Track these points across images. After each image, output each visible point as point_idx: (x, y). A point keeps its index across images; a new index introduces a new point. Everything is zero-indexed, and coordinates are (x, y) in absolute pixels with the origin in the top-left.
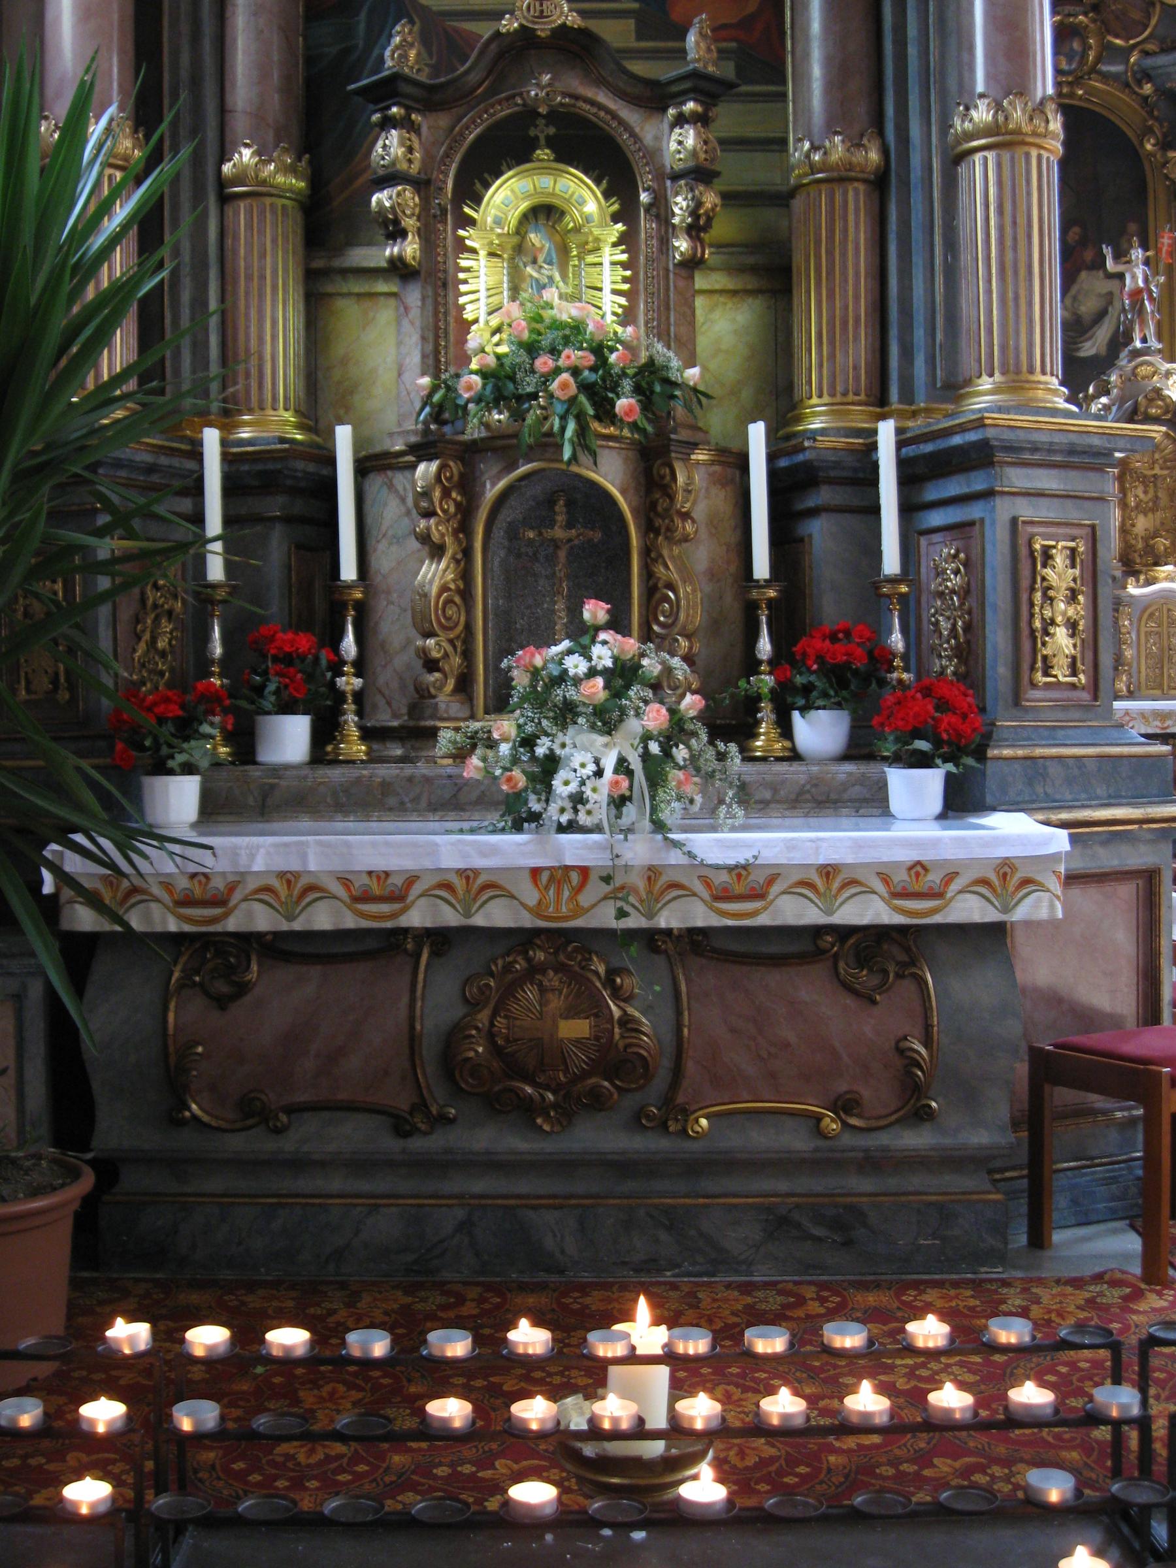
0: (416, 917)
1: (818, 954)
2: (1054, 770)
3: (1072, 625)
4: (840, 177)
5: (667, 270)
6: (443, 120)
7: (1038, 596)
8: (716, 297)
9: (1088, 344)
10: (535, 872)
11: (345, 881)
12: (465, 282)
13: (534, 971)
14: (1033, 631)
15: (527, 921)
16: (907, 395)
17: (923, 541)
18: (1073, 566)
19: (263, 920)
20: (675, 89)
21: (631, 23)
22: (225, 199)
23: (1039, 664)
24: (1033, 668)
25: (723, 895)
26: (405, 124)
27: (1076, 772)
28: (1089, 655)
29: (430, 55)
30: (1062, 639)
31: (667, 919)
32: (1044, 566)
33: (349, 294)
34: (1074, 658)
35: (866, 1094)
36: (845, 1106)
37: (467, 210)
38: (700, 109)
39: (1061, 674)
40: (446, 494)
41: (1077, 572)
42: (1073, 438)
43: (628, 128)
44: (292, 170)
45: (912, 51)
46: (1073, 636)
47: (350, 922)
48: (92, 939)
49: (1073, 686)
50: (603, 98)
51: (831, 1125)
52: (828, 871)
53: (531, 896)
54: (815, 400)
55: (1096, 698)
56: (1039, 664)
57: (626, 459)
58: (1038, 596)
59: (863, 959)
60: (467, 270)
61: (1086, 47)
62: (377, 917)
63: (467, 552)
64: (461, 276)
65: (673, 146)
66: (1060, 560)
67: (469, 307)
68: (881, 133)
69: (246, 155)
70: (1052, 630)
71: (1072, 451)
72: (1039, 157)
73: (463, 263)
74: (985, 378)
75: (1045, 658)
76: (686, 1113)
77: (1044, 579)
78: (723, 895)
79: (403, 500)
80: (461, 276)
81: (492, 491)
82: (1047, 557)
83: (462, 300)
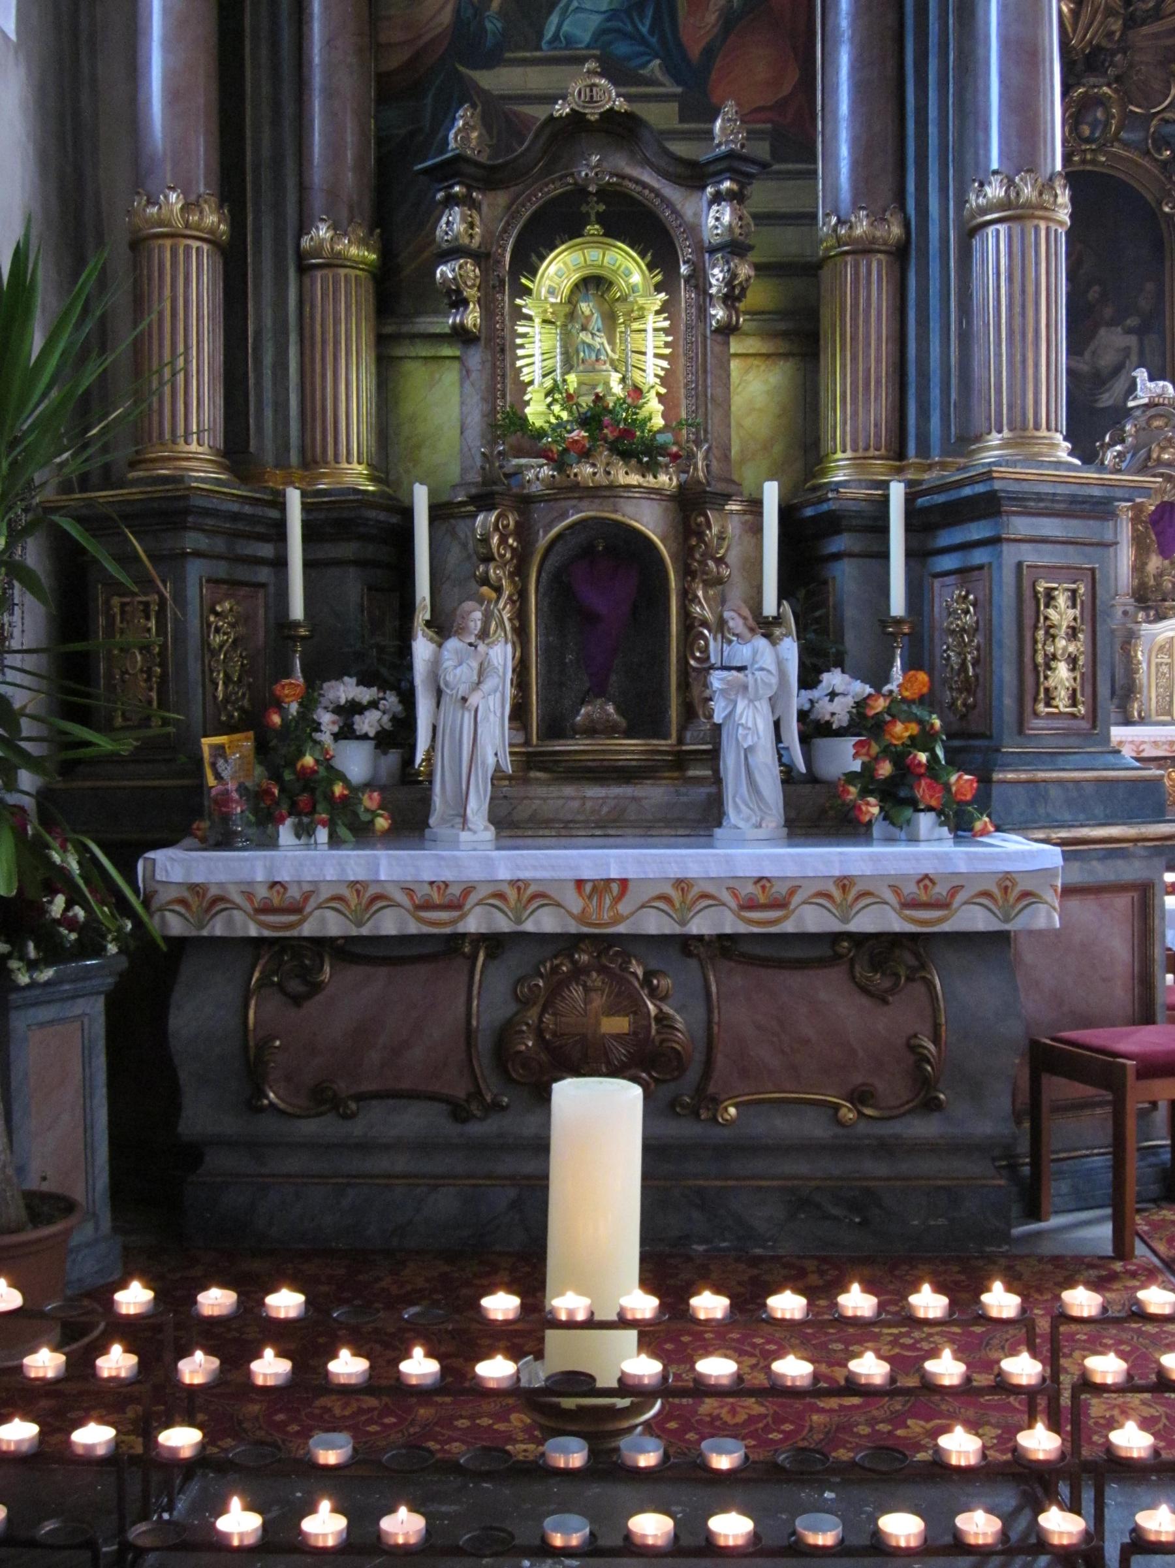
0: (472, 924)
1: (834, 959)
2: (1054, 792)
3: (1073, 661)
4: (864, 249)
5: (705, 337)
6: (502, 198)
7: (1041, 634)
8: (750, 360)
9: (1106, 396)
10: (580, 883)
11: (409, 891)
12: (522, 346)
13: (579, 972)
14: (1036, 666)
15: (573, 928)
16: (924, 449)
17: (937, 583)
18: (1074, 606)
19: (334, 925)
20: (712, 169)
21: (675, 106)
22: (304, 269)
23: (1042, 695)
24: (1036, 700)
25: (751, 905)
26: (467, 201)
27: (1075, 794)
28: (1088, 689)
29: (491, 138)
30: (1062, 670)
31: (700, 926)
32: (1047, 606)
33: (417, 358)
34: (1074, 690)
35: (880, 1086)
36: (860, 1097)
37: (524, 281)
38: (735, 187)
39: (1062, 703)
40: (503, 540)
41: (1077, 612)
42: (1073, 490)
43: (670, 204)
44: (363, 243)
45: (933, 130)
46: (1073, 670)
47: (413, 928)
48: (179, 944)
49: (1073, 716)
50: (648, 177)
51: (848, 1114)
52: (844, 883)
53: (575, 903)
54: (839, 455)
55: (1094, 727)
56: (1042, 695)
57: (666, 509)
58: (1041, 634)
59: (876, 965)
60: (524, 335)
61: (1108, 116)
62: (440, 922)
63: (522, 594)
64: (519, 341)
65: (711, 222)
66: (1062, 600)
67: (525, 370)
68: (902, 207)
69: (323, 232)
70: (1053, 664)
71: (1073, 499)
72: (1048, 229)
73: (521, 330)
74: (994, 434)
75: (1047, 690)
76: (715, 1102)
77: (1046, 618)
78: (751, 905)
79: (464, 546)
80: (519, 341)
81: (543, 541)
82: (1050, 597)
83: (519, 363)
